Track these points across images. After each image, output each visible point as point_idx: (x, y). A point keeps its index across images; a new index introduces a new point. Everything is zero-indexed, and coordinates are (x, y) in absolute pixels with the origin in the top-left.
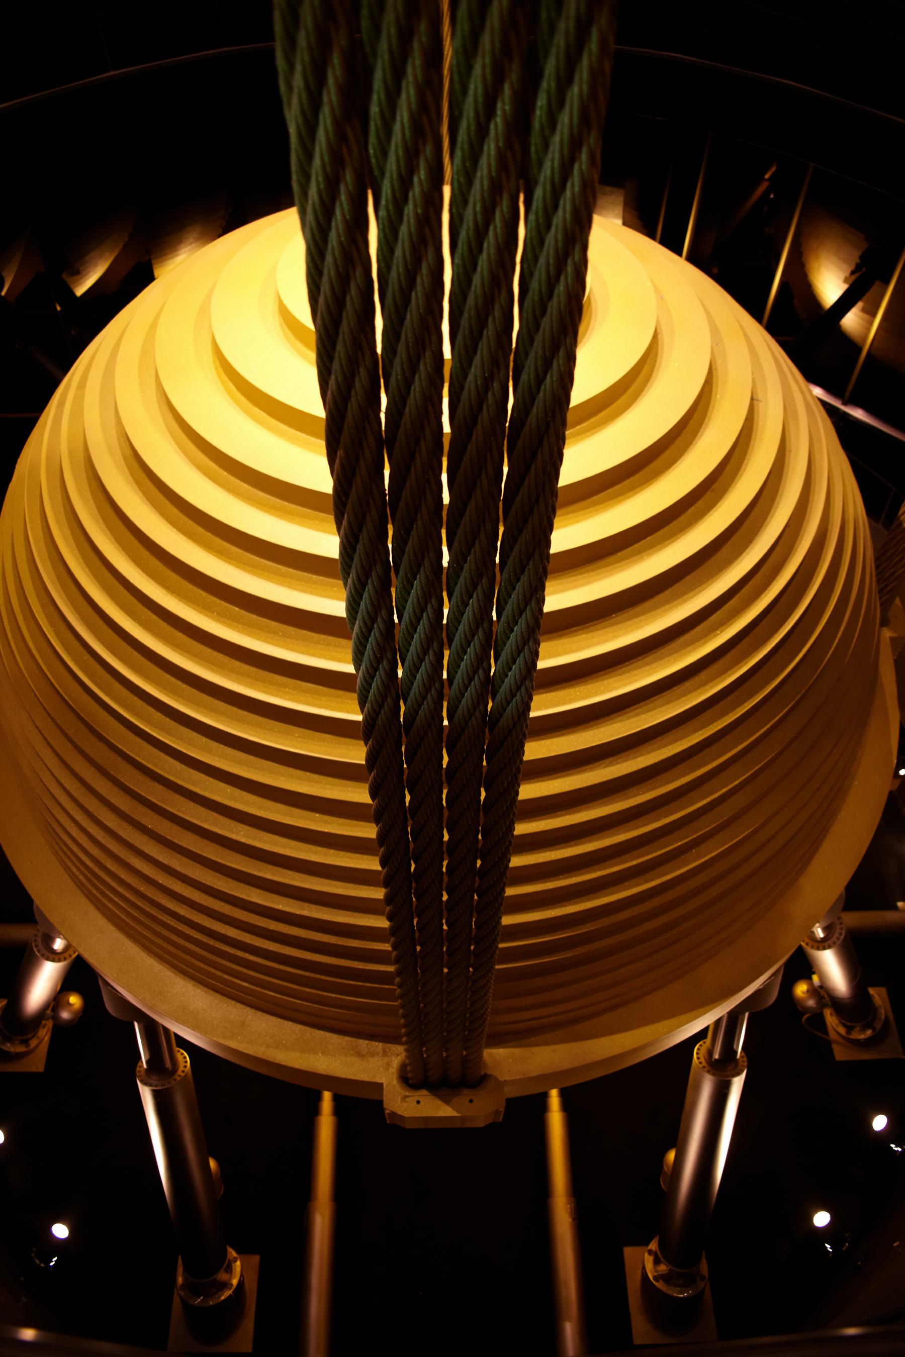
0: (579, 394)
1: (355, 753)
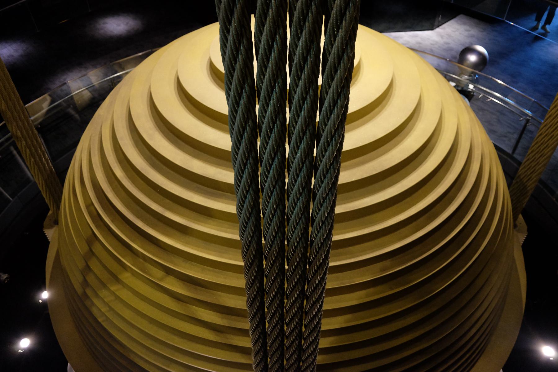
0: (353, 107)
1: (240, 282)
